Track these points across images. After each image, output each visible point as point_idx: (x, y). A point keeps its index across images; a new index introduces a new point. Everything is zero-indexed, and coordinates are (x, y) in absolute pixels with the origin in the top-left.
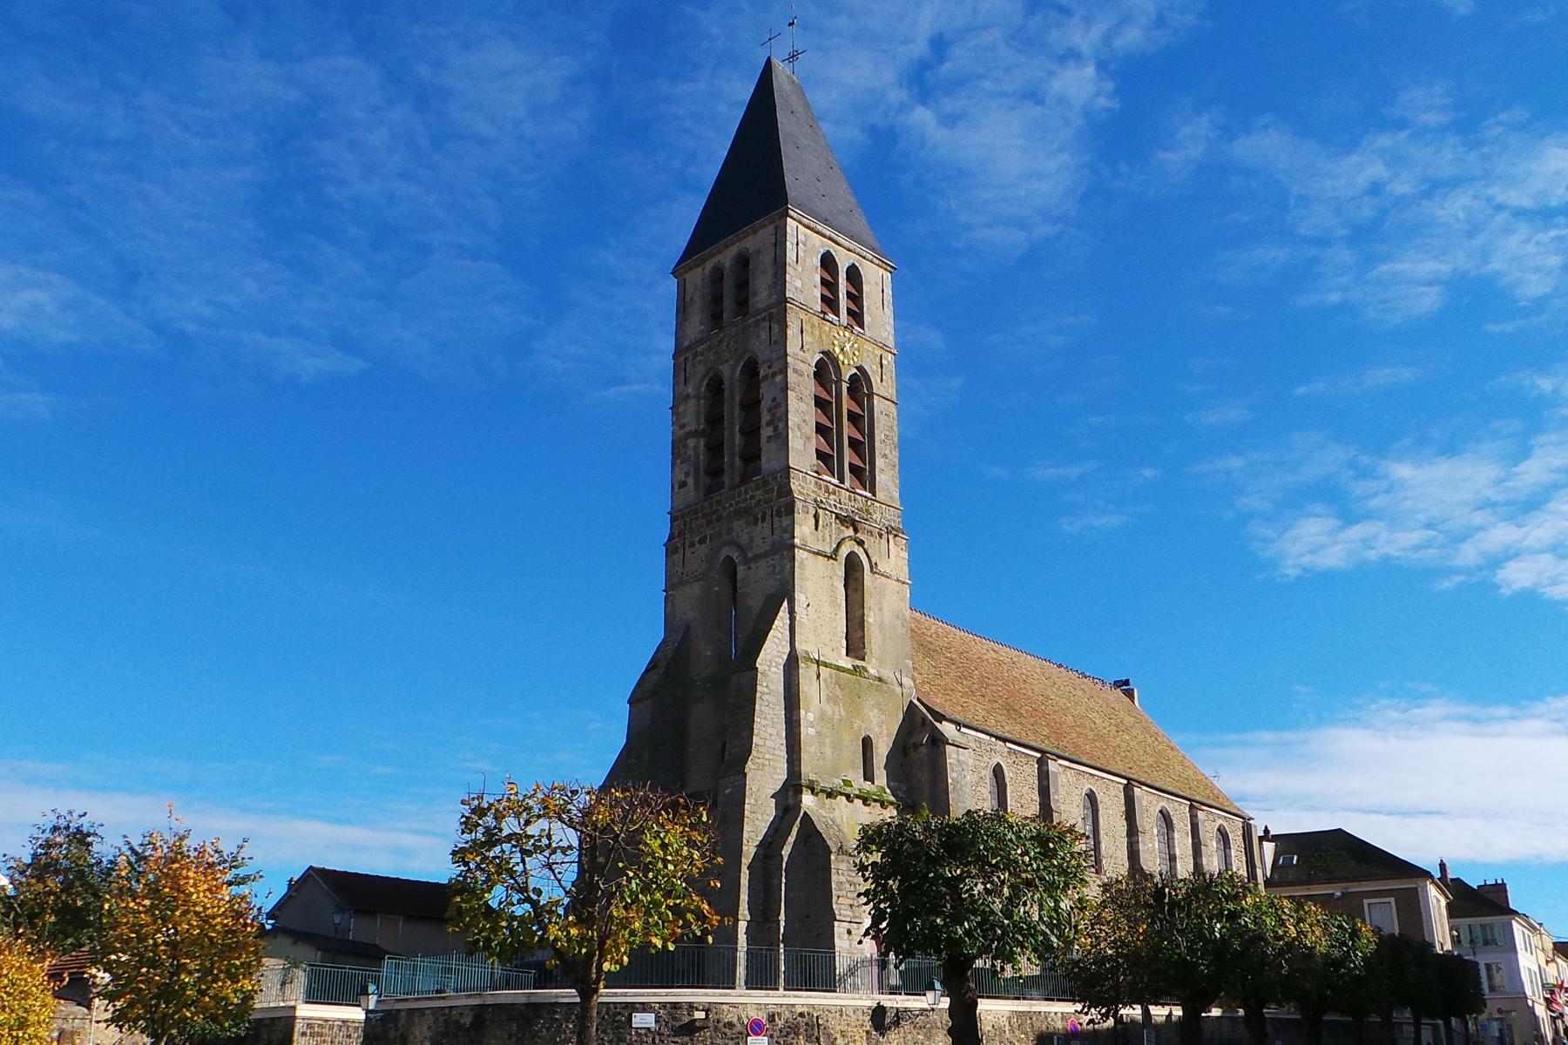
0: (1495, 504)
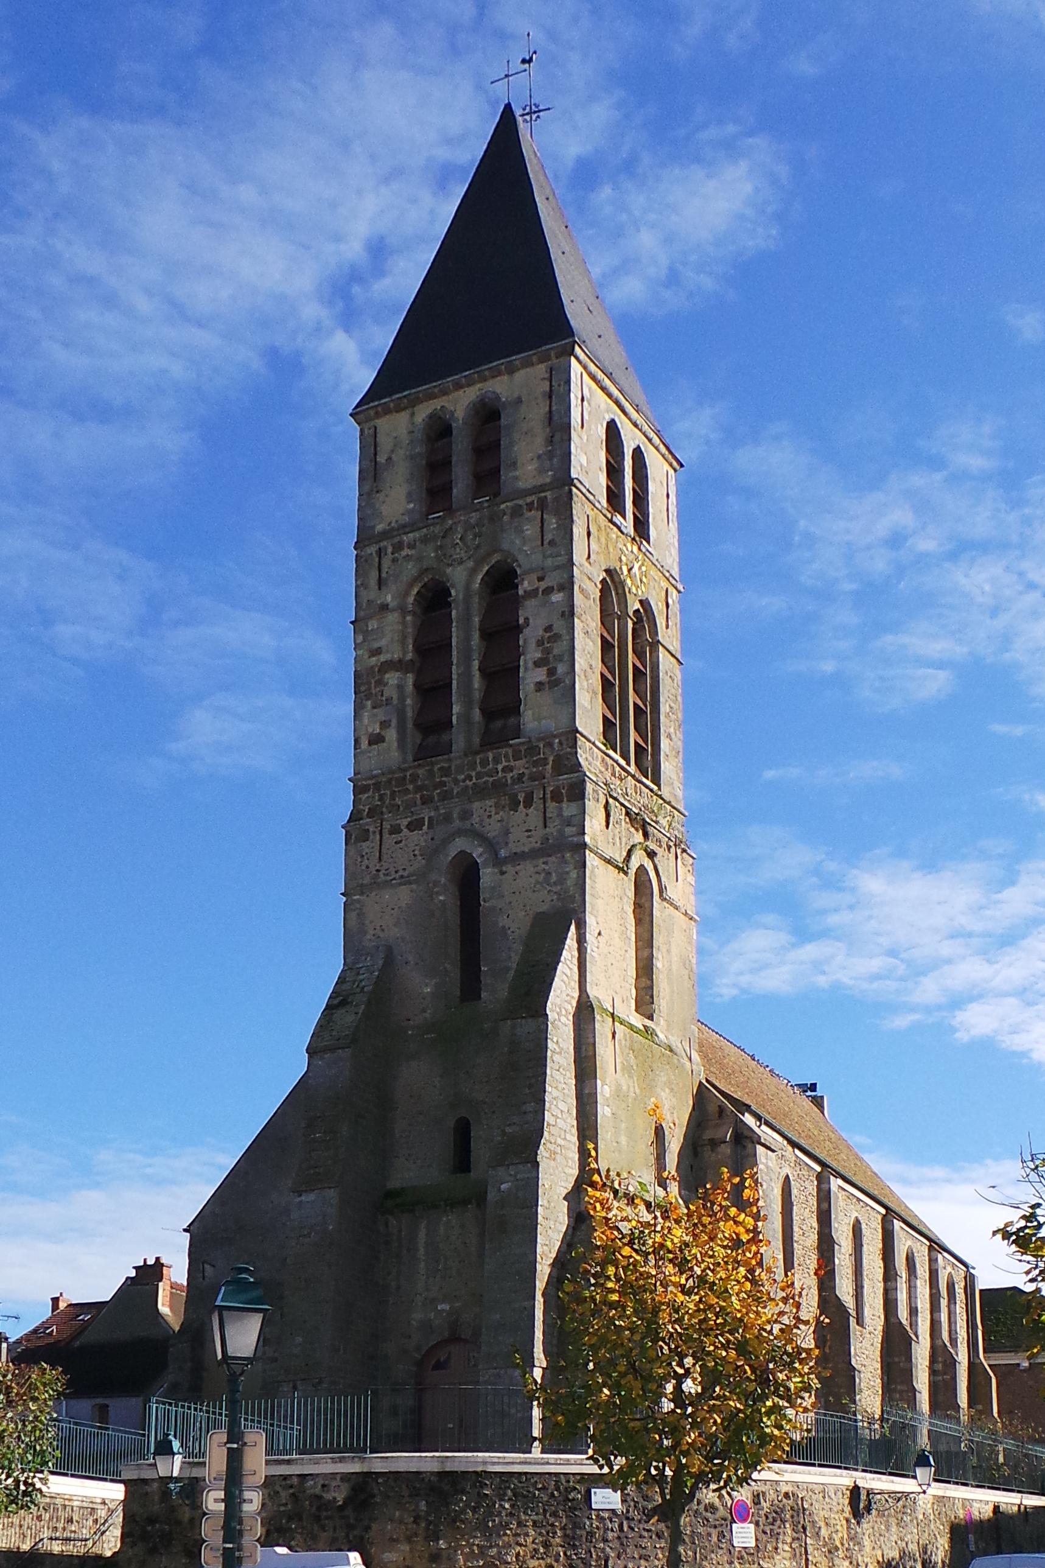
0: (970, 935)
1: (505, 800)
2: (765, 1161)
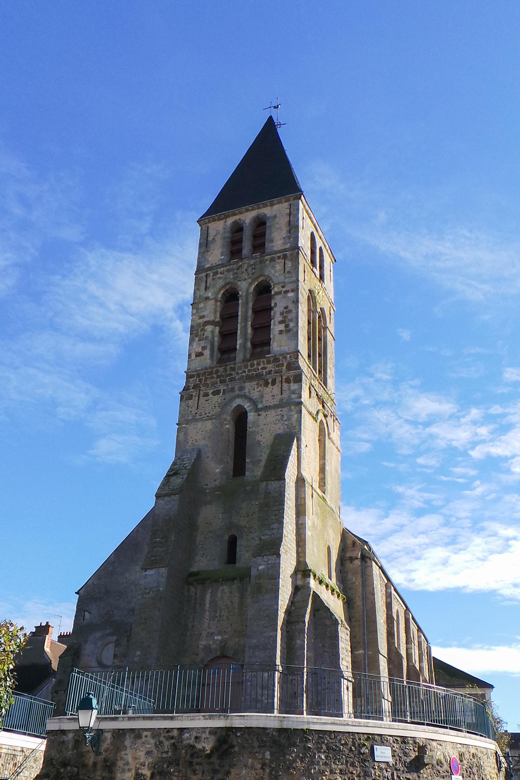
1: (261, 382)
2: (375, 570)
